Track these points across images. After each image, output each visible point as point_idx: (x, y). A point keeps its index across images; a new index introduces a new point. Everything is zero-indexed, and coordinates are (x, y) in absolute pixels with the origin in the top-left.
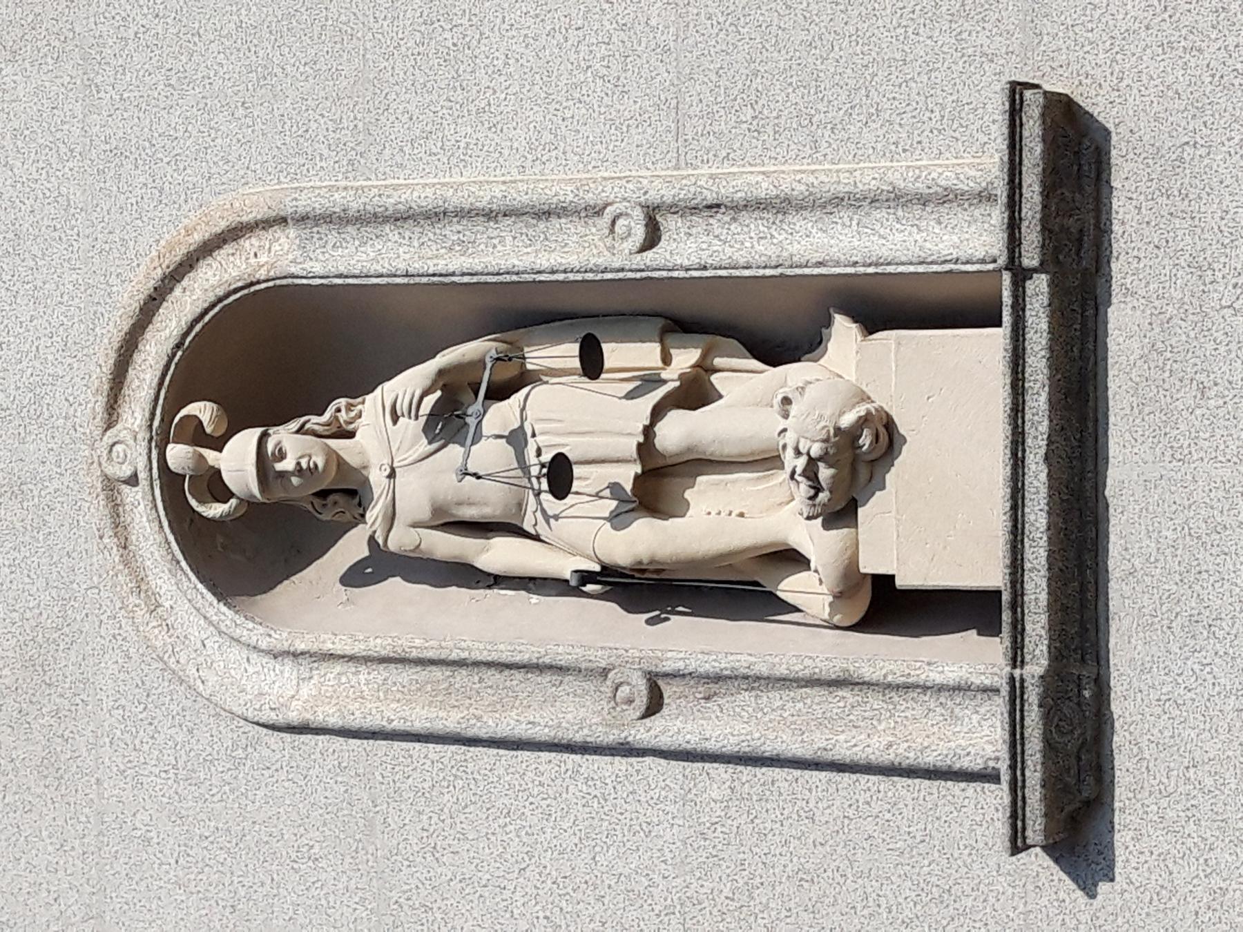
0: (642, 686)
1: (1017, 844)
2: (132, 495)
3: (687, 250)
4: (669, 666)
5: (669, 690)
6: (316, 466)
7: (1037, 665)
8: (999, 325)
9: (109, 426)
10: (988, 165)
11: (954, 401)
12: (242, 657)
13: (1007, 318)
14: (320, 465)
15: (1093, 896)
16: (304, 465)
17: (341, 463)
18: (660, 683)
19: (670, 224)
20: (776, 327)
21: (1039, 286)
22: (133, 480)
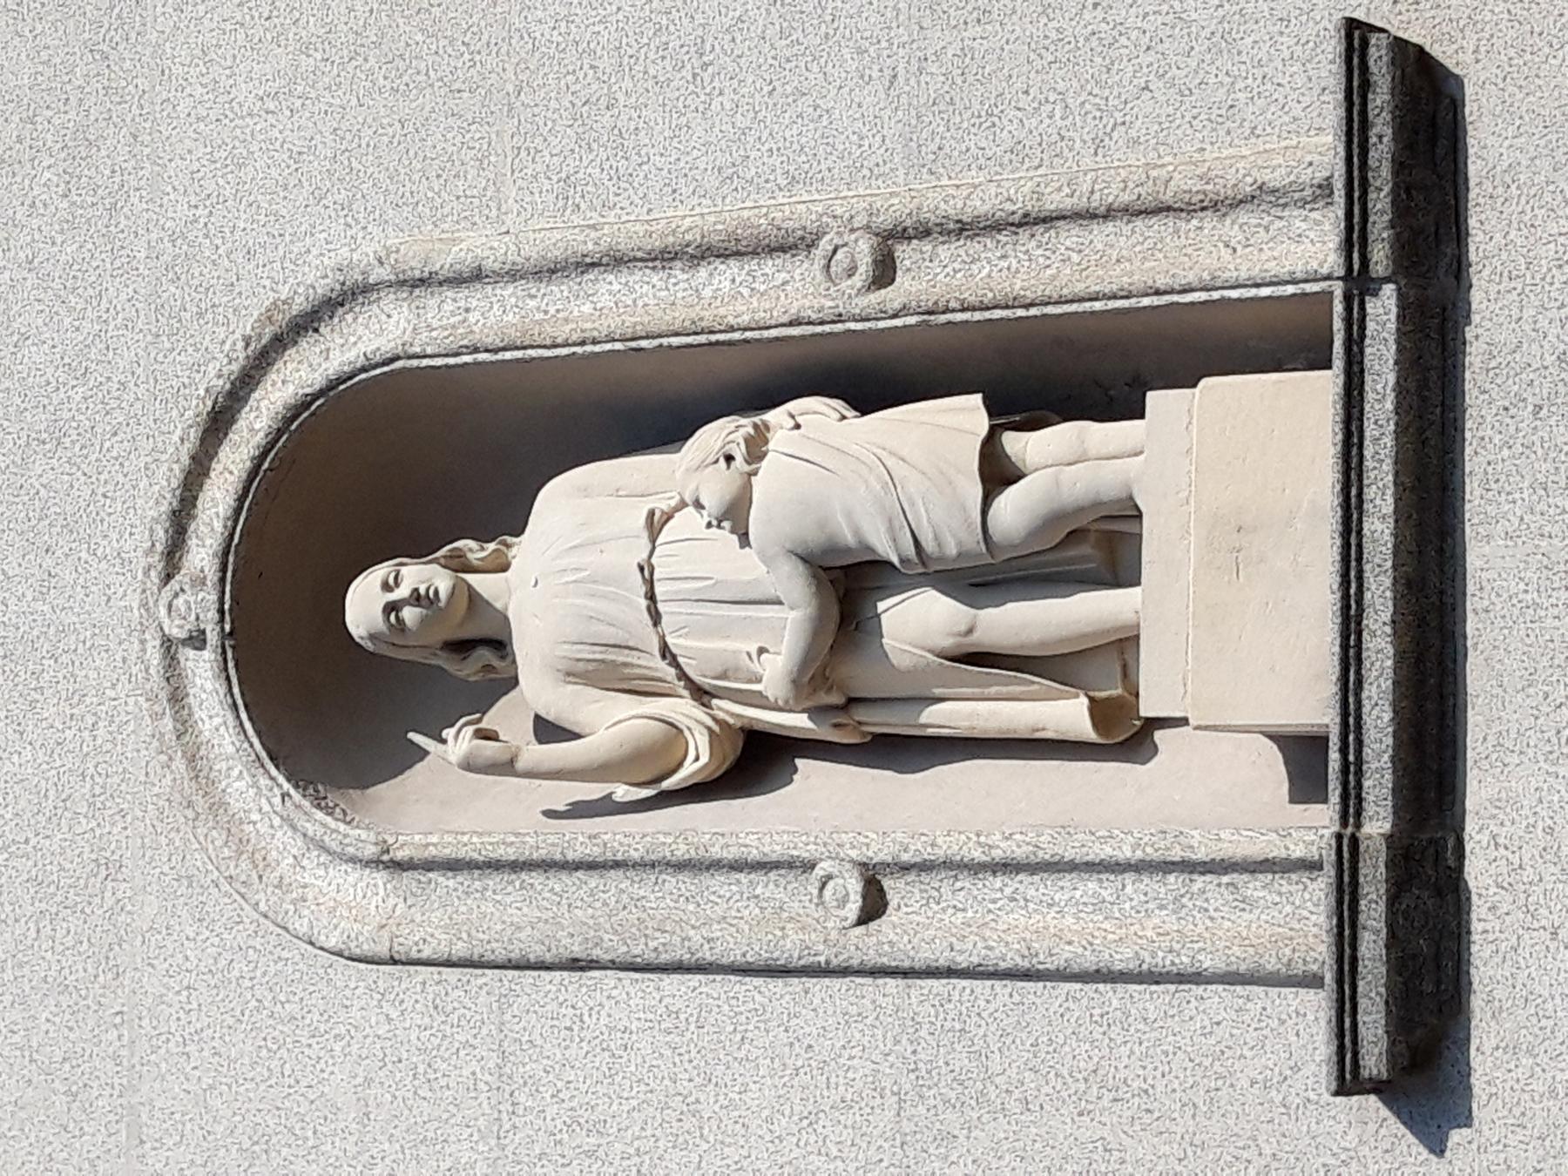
0: (855, 886)
1: (1348, 1081)
2: (188, 656)
3: (937, 280)
4: (884, 856)
5: (893, 887)
6: (436, 592)
7: (1377, 824)
8: (1330, 367)
9: (168, 577)
10: (1322, 150)
11: (1238, 485)
12: (307, 861)
13: (1338, 363)
14: (443, 595)
15: (1438, 1149)
16: (422, 591)
17: (473, 596)
18: (887, 883)
19: (905, 254)
20: (463, 834)
21: (1383, 309)
22: (197, 640)
